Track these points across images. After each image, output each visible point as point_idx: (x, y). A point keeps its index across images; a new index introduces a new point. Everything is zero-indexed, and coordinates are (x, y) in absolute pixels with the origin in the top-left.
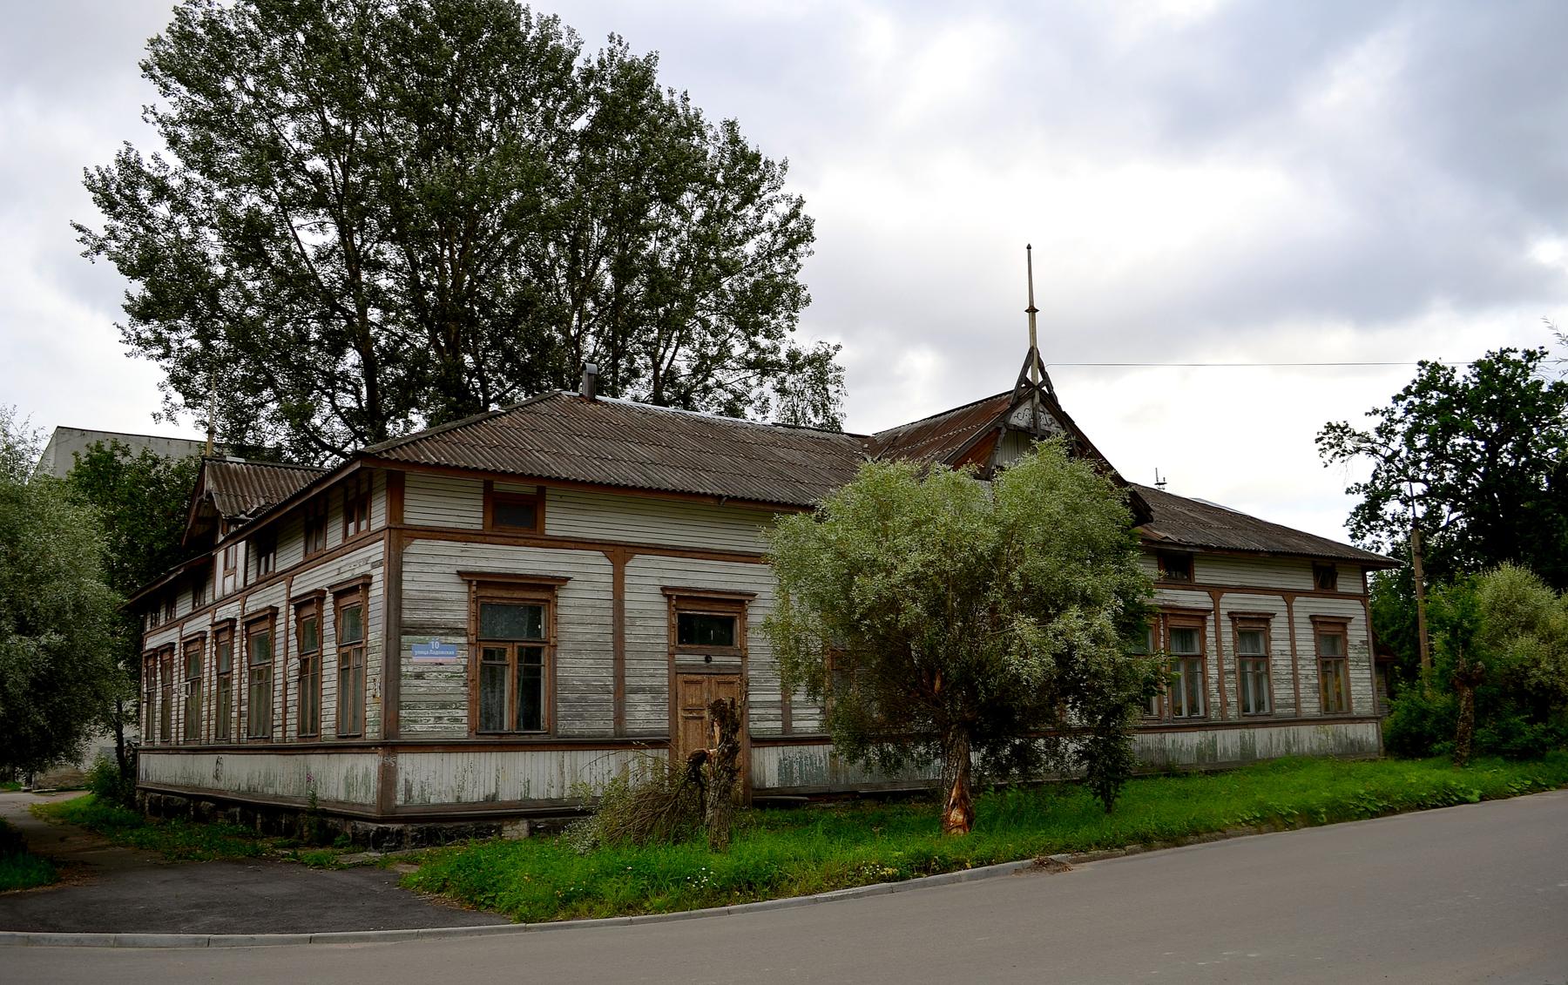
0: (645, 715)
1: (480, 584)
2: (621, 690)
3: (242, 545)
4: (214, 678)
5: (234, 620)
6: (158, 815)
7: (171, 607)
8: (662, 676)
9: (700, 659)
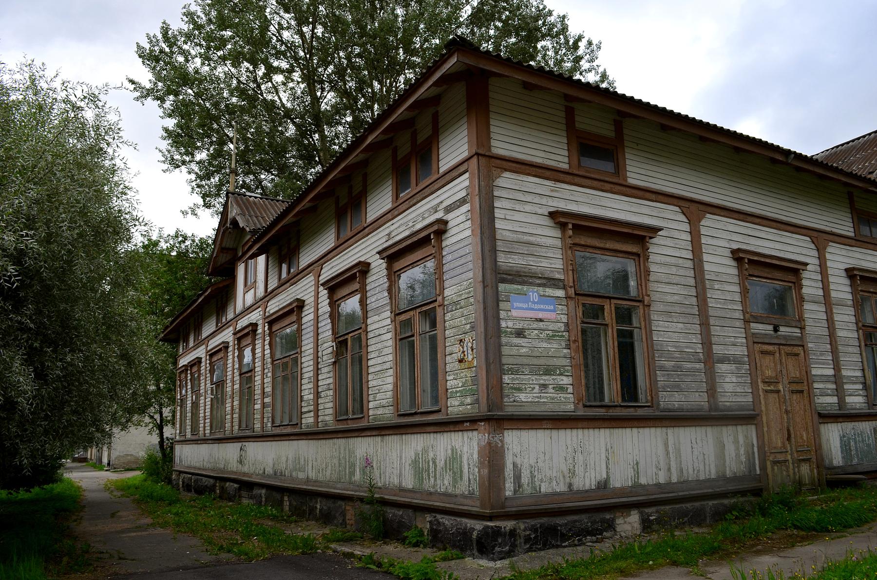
0: (733, 388)
1: (576, 227)
2: (710, 359)
3: (262, 259)
4: (237, 378)
5: (256, 325)
6: (189, 490)
7: (198, 329)
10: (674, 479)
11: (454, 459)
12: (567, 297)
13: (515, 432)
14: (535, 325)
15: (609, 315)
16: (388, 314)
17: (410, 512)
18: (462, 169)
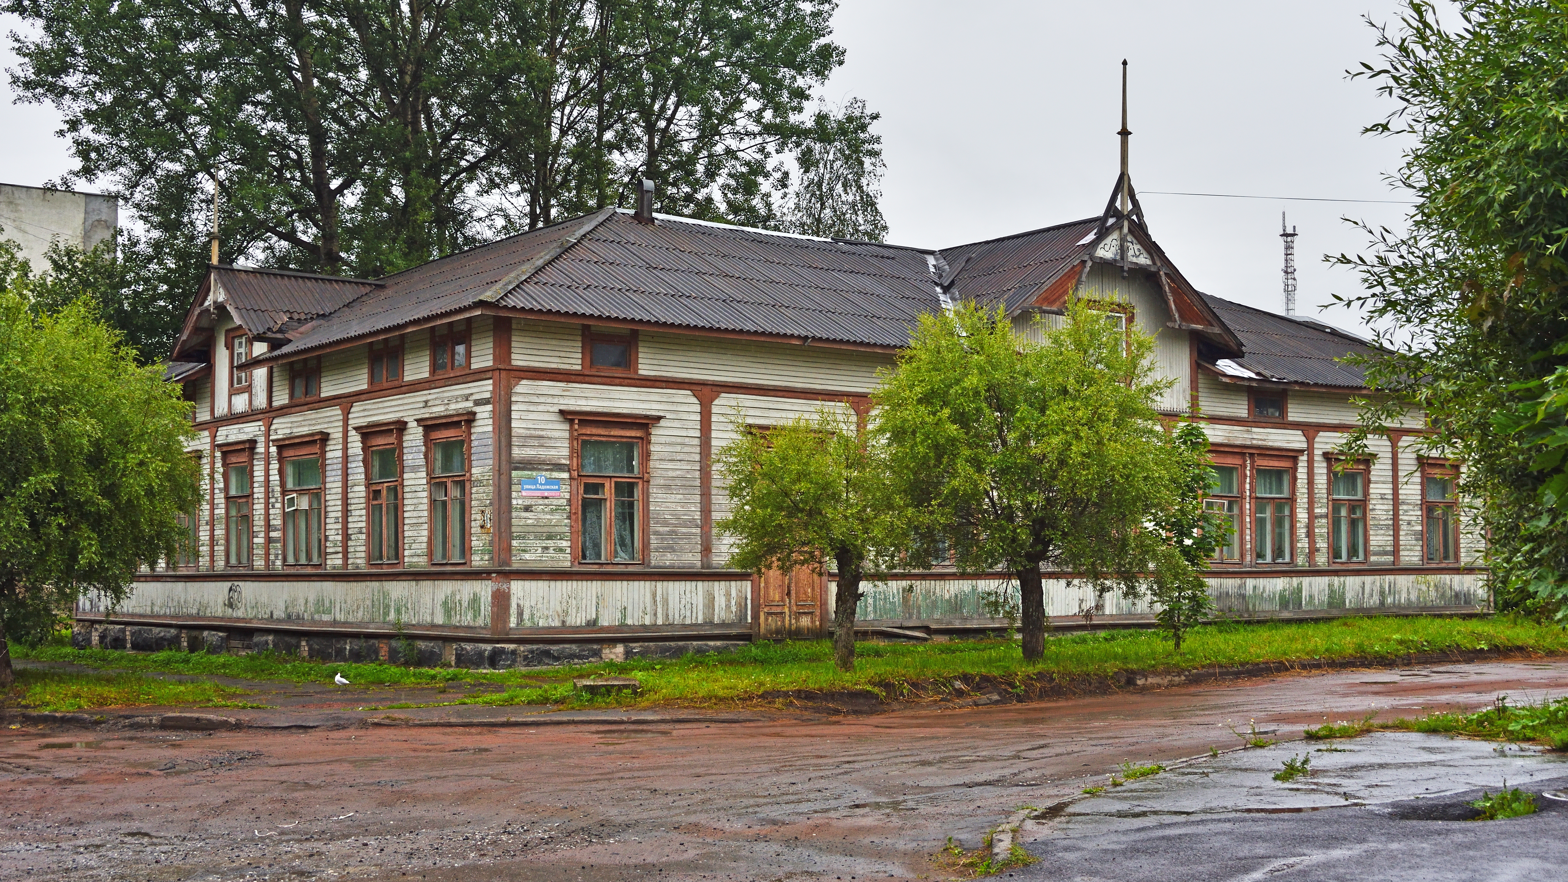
10: (660, 622)
11: (475, 601)
12: (571, 478)
13: (520, 583)
14: (541, 502)
15: (608, 492)
16: (424, 474)
17: (440, 643)
18: (489, 375)
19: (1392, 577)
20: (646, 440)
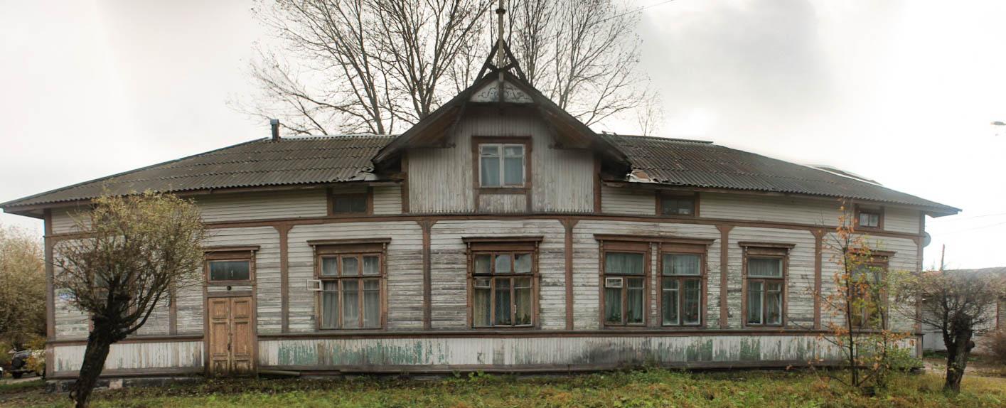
8: (199, 300)
9: (224, 289)
10: (144, 366)
19: (812, 338)
20: (786, 257)
